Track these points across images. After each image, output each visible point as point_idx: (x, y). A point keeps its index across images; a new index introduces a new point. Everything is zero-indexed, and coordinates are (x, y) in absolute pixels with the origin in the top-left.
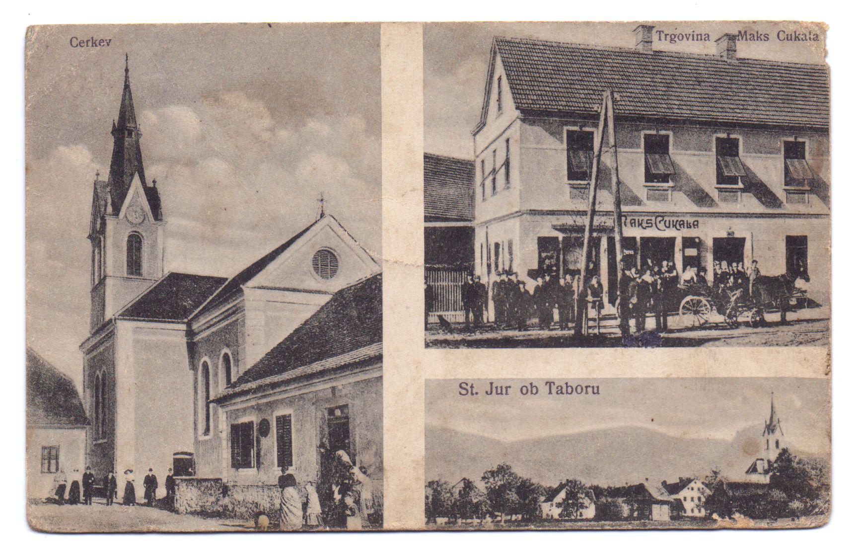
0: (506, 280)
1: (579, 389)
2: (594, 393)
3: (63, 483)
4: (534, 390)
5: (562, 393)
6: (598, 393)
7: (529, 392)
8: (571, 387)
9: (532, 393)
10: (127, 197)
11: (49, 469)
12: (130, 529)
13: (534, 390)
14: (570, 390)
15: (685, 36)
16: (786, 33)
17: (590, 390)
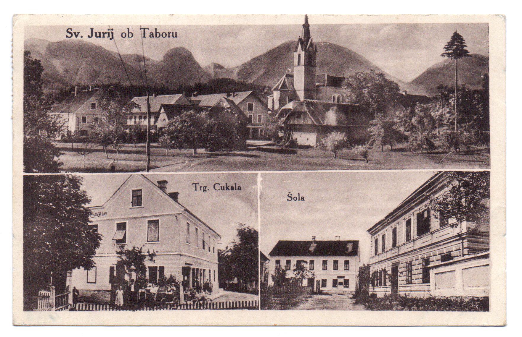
0: (226, 105)
1: (164, 35)
2: (173, 36)
3: (115, 241)
4: (130, 35)
5: (153, 37)
6: (176, 37)
7: (127, 36)
8: (159, 33)
9: (129, 37)
10: (416, 229)
11: (193, 308)
12: (211, 231)
13: (130, 35)
14: (158, 35)
15: (74, 34)
16: (221, 185)
17: (171, 35)
